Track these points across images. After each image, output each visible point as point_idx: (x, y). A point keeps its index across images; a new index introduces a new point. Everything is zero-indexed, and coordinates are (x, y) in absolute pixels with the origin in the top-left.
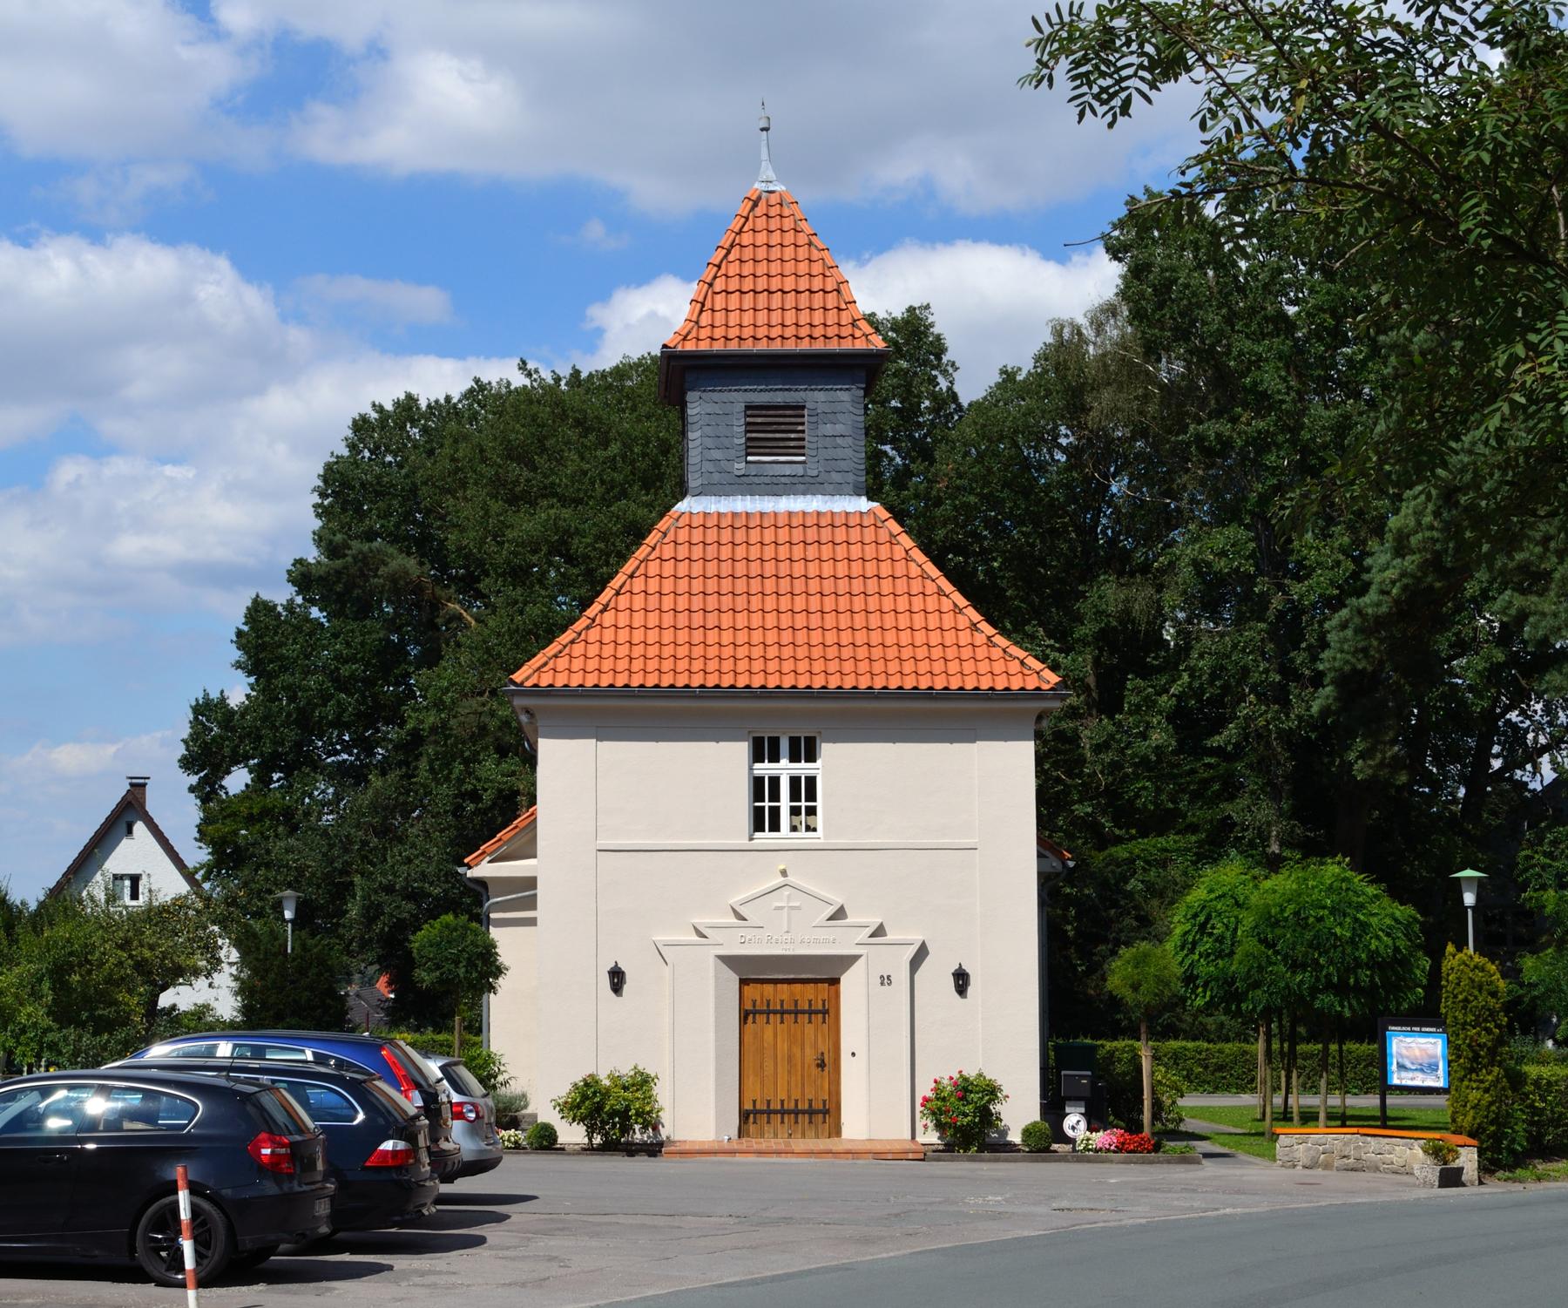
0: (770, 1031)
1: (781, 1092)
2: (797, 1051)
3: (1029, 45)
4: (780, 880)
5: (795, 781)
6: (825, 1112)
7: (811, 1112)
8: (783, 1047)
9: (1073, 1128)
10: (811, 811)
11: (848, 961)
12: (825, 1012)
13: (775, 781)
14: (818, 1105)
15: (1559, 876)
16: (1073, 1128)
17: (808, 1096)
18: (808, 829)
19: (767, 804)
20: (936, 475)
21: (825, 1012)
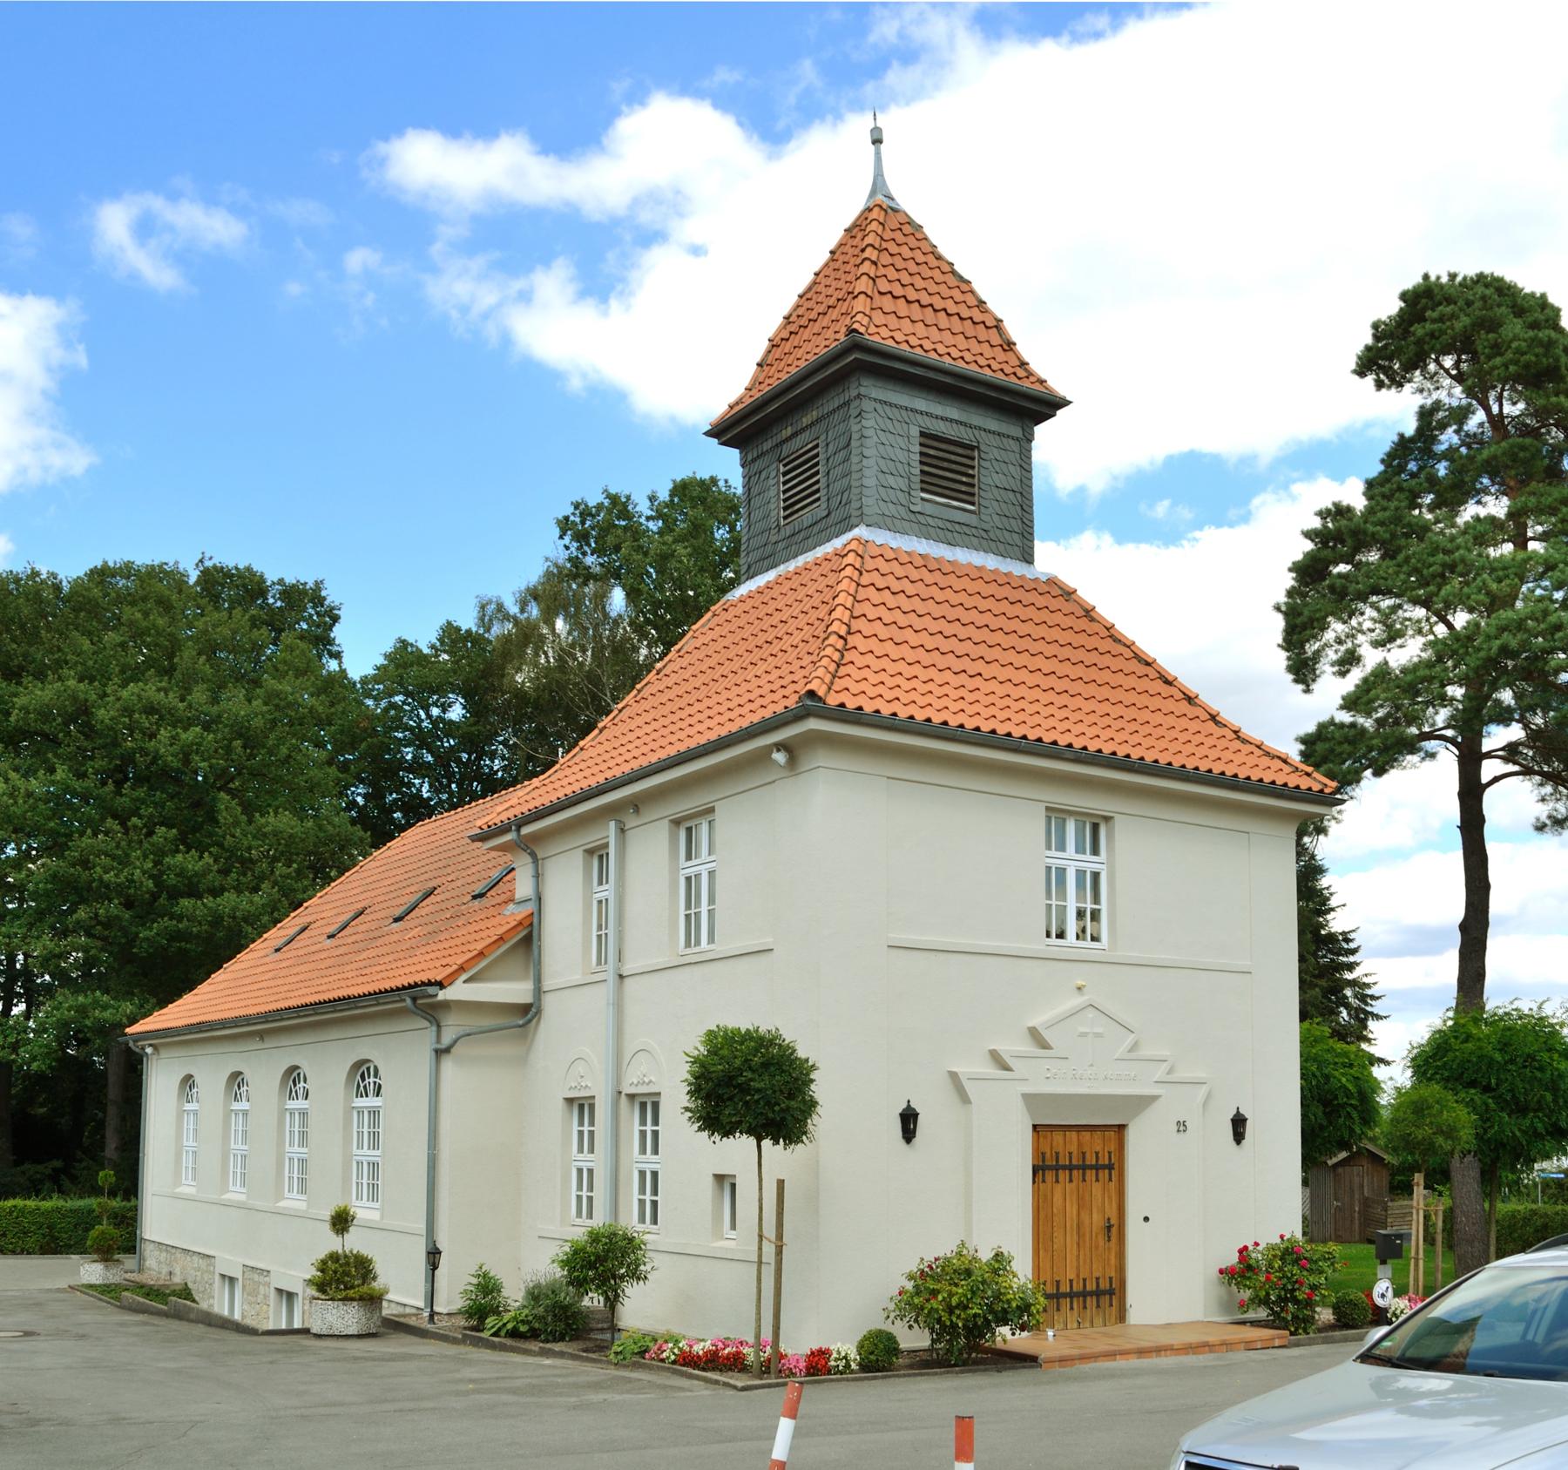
0: (1064, 1192)
1: (1069, 1273)
2: (1085, 1217)
3: (697, 251)
4: (1078, 1001)
5: (1080, 874)
6: (1111, 1292)
7: (1098, 1293)
8: (1072, 1210)
9: (1383, 1296)
10: (1095, 916)
11: (1143, 1102)
12: (1110, 1167)
13: (1062, 872)
14: (1104, 1285)
15: (4, 1235)
16: (1383, 1296)
17: (1096, 1274)
18: (1094, 939)
19: (1054, 902)
20: (74, 865)
21: (1110, 1167)
